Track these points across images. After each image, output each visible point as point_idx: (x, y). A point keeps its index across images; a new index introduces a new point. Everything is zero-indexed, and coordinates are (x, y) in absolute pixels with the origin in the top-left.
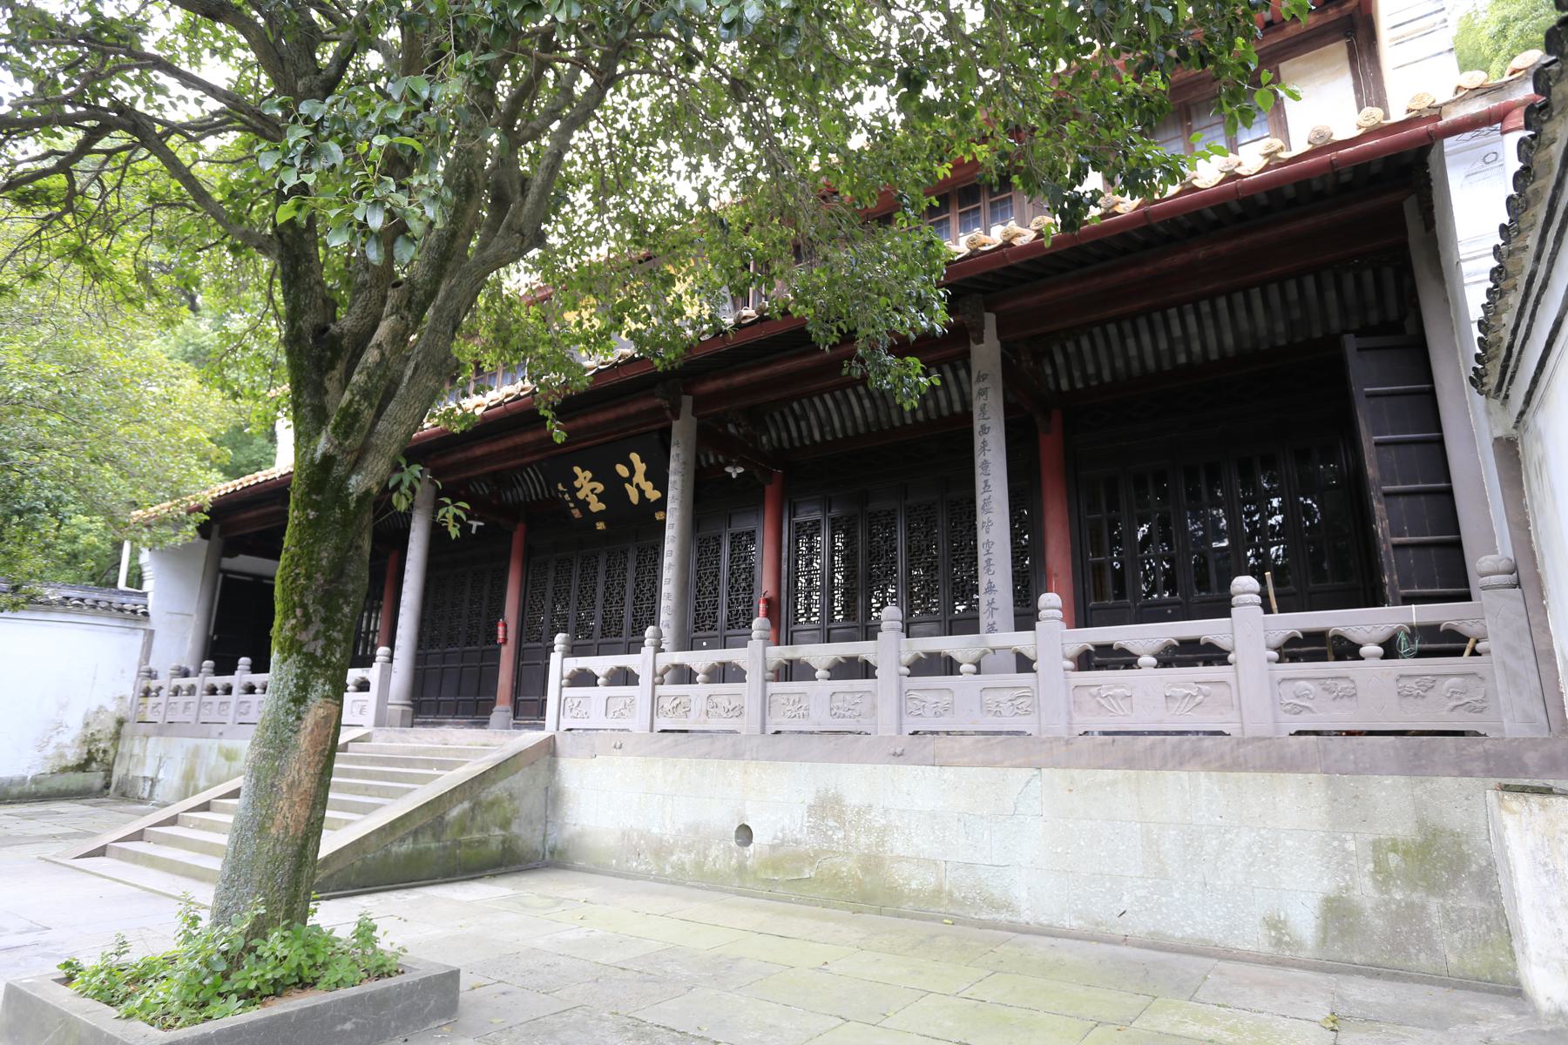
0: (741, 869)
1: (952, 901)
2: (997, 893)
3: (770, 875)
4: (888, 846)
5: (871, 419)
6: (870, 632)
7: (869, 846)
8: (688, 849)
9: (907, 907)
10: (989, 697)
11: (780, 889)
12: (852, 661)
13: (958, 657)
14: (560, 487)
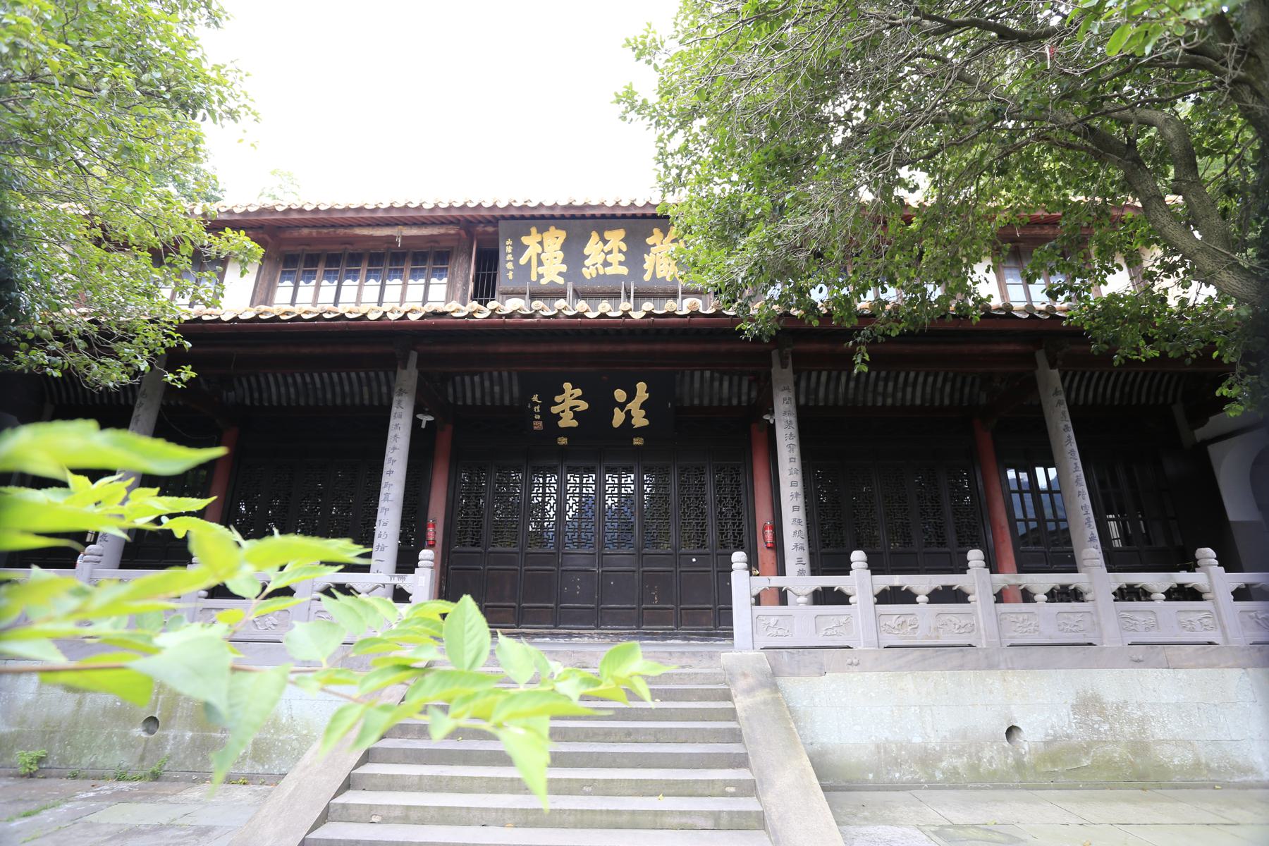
0: (1020, 766)
1: (1210, 770)
2: (1240, 760)
3: (1049, 767)
4: (1149, 733)
5: (851, 396)
6: (845, 569)
7: (1133, 734)
8: (959, 754)
9: (1177, 779)
10: (1183, 617)
11: (1062, 779)
12: (947, 589)
13: (915, 590)
14: (535, 398)
